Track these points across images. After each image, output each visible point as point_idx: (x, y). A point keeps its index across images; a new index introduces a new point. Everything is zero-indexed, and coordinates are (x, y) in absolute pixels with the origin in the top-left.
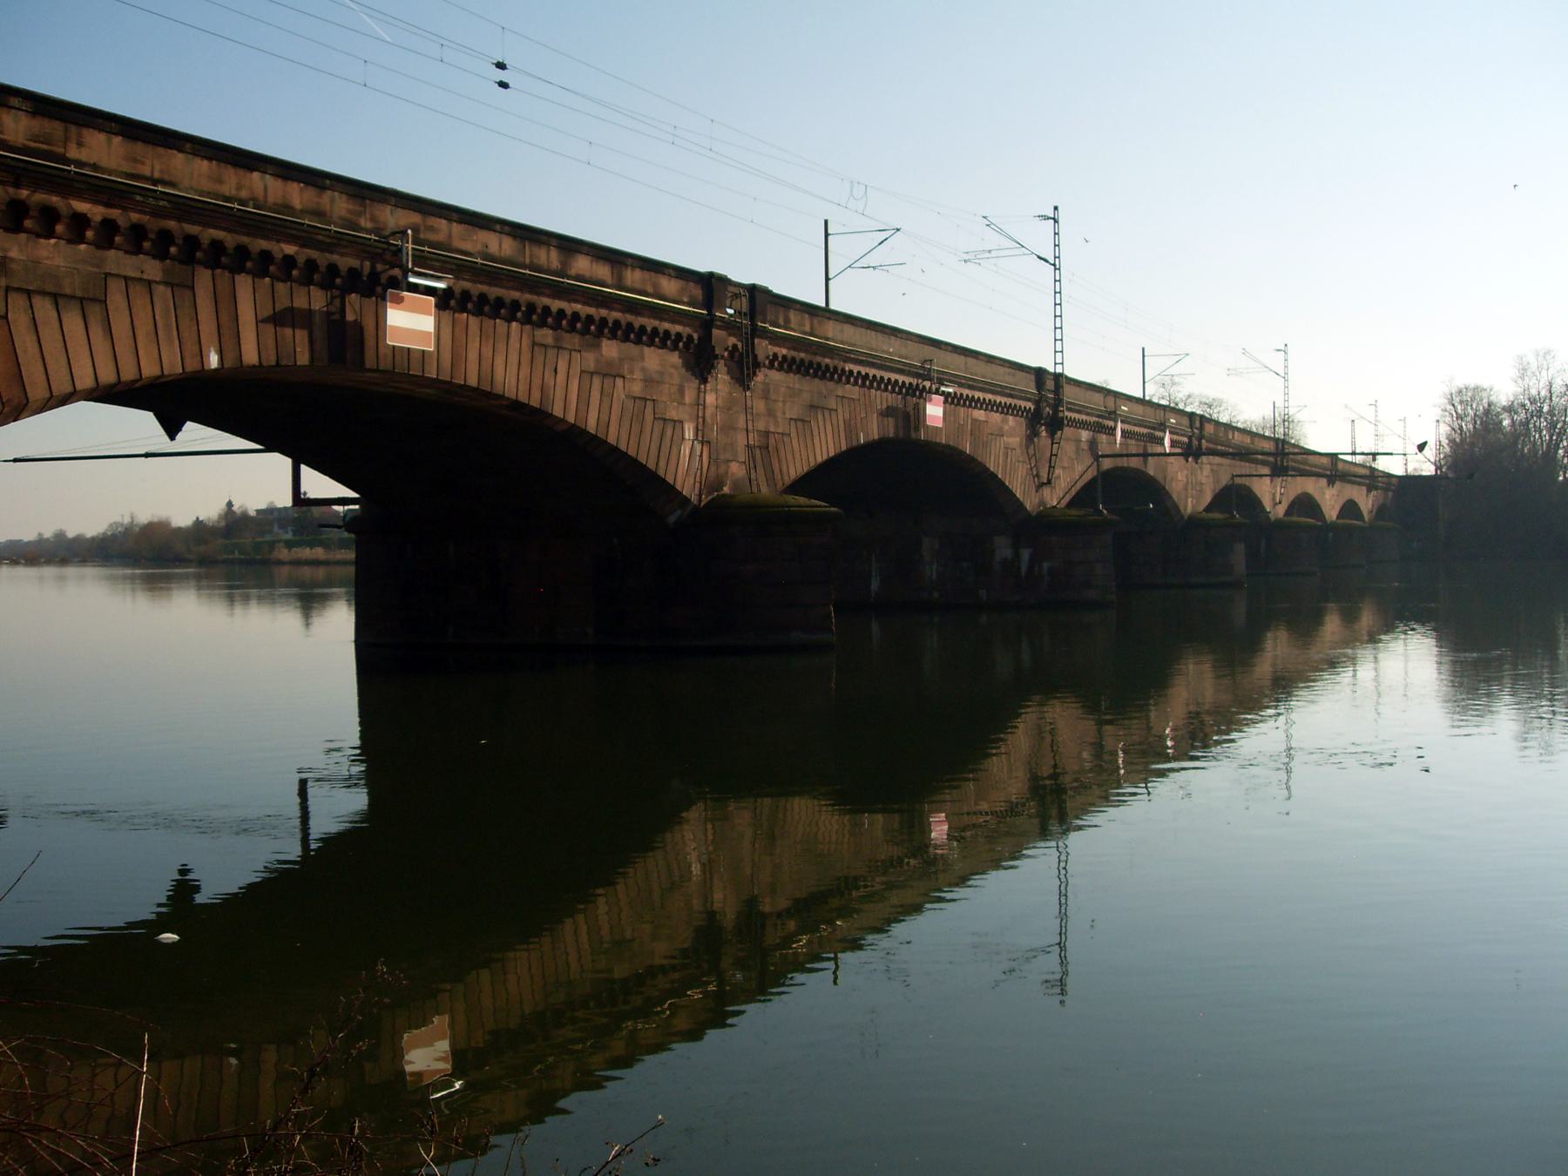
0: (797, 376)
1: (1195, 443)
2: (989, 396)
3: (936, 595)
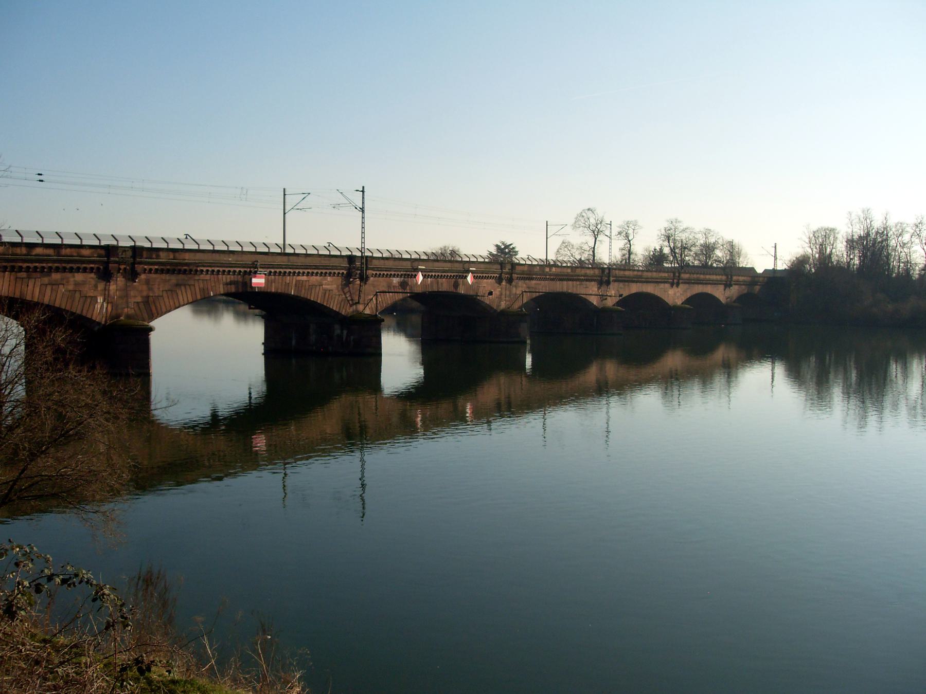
0: (167, 275)
3: (314, 348)
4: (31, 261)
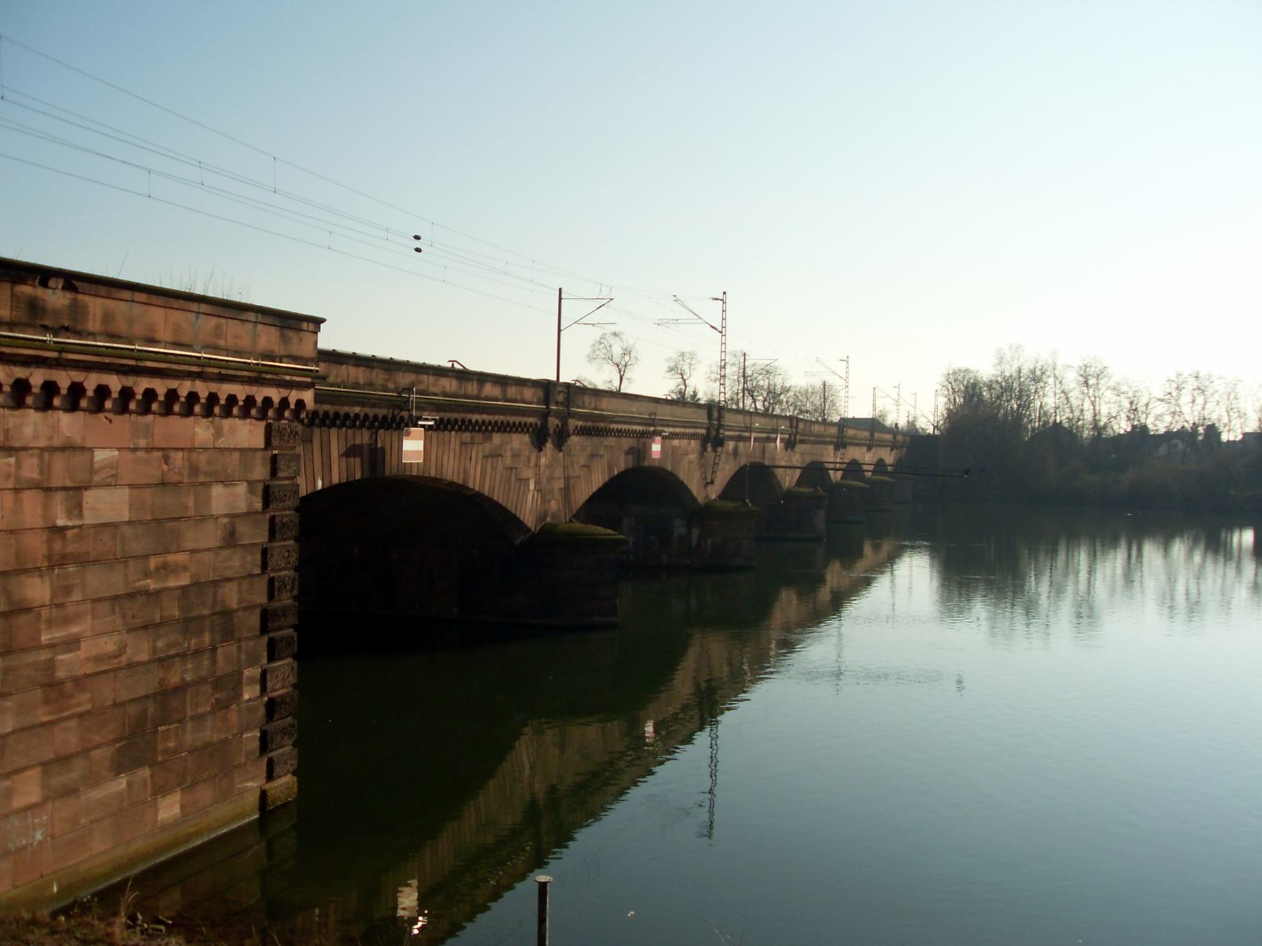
1: (793, 438)
2: (682, 430)
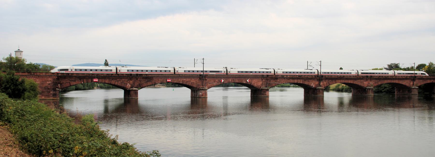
4: (112, 77)
